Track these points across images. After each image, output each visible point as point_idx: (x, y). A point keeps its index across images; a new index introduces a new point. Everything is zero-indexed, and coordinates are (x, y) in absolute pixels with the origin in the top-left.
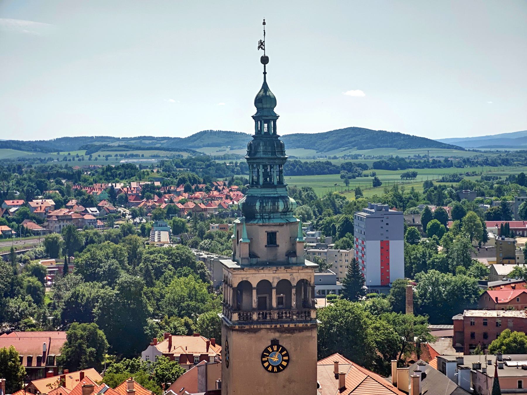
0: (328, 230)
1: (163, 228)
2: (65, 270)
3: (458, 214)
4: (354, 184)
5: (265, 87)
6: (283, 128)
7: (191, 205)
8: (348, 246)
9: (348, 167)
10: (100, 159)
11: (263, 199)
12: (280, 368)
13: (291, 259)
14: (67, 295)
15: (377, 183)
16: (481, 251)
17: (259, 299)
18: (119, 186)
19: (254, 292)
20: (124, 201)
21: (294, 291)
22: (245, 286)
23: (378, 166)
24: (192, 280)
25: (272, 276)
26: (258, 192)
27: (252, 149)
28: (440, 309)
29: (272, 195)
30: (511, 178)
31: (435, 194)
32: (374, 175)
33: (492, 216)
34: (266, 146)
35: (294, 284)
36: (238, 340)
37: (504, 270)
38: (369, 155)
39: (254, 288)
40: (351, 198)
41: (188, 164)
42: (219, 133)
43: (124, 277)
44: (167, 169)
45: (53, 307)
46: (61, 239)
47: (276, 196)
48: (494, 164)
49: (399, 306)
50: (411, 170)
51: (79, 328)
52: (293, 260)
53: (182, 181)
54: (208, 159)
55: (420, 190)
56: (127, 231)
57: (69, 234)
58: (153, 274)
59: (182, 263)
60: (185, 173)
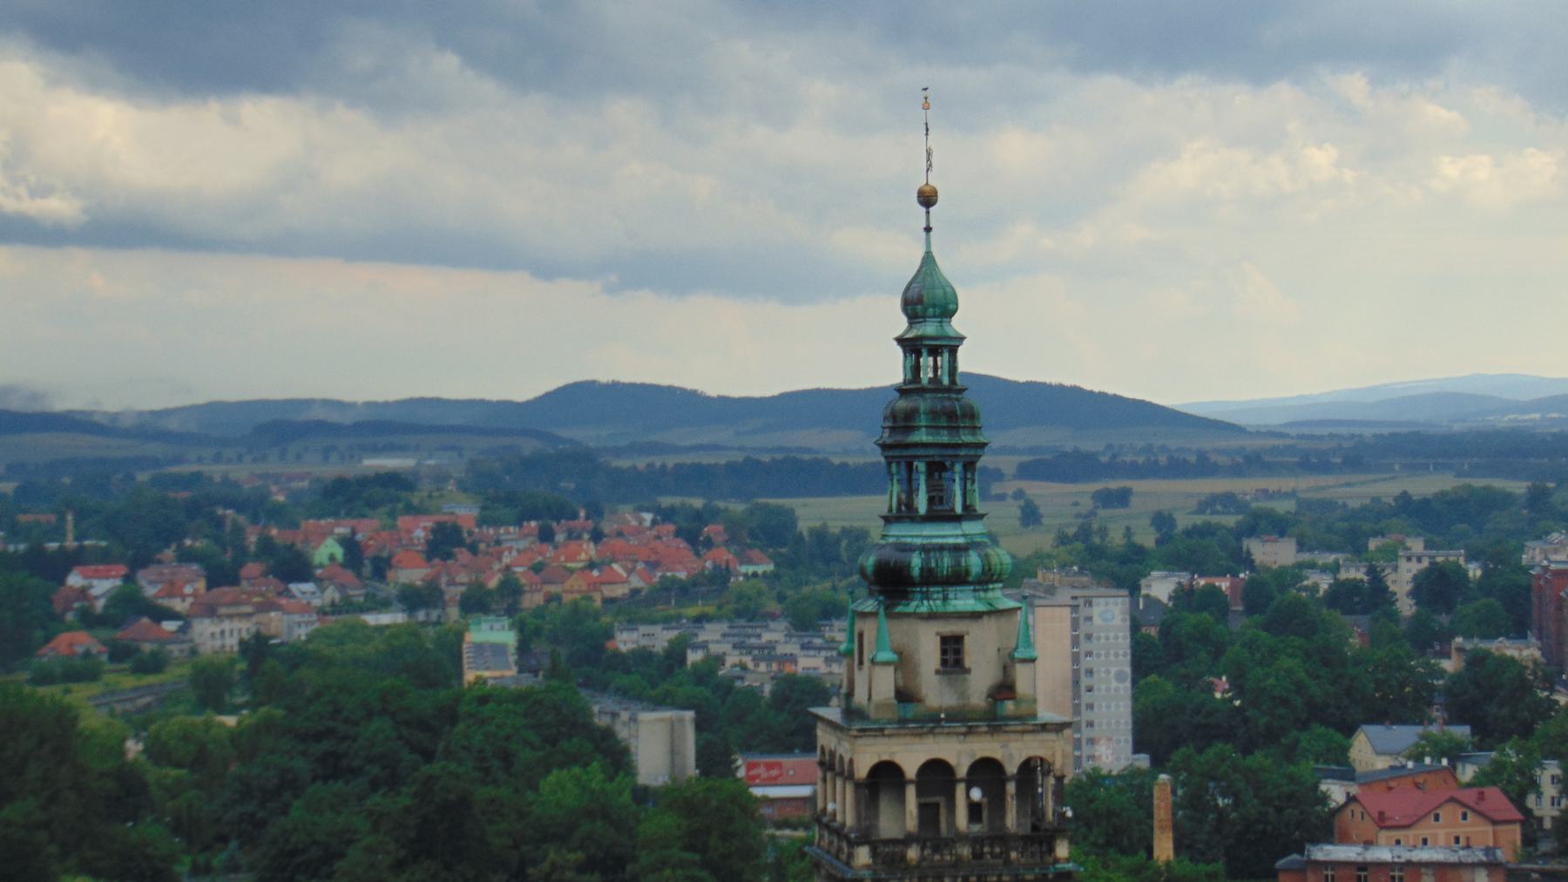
5: (928, 259)
17: (922, 807)
19: (911, 792)
21: (1011, 788)
25: (959, 753)
29: (951, 541)
32: (1019, 494)
35: (1012, 769)
39: (911, 782)
47: (961, 541)
48: (1236, 471)
50: (1114, 485)
52: (1009, 706)
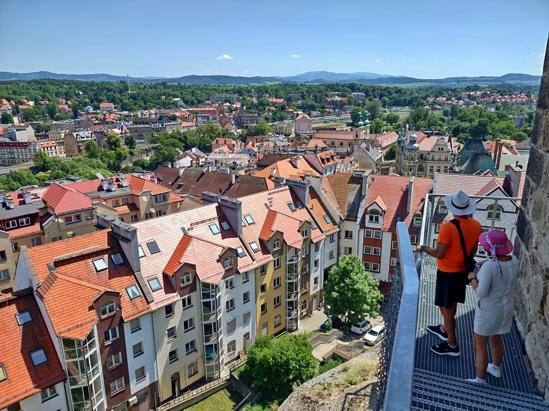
1: (492, 107)
7: (503, 100)
10: (463, 85)
18: (472, 93)
42: (516, 74)
46: (450, 110)
54: (510, 84)
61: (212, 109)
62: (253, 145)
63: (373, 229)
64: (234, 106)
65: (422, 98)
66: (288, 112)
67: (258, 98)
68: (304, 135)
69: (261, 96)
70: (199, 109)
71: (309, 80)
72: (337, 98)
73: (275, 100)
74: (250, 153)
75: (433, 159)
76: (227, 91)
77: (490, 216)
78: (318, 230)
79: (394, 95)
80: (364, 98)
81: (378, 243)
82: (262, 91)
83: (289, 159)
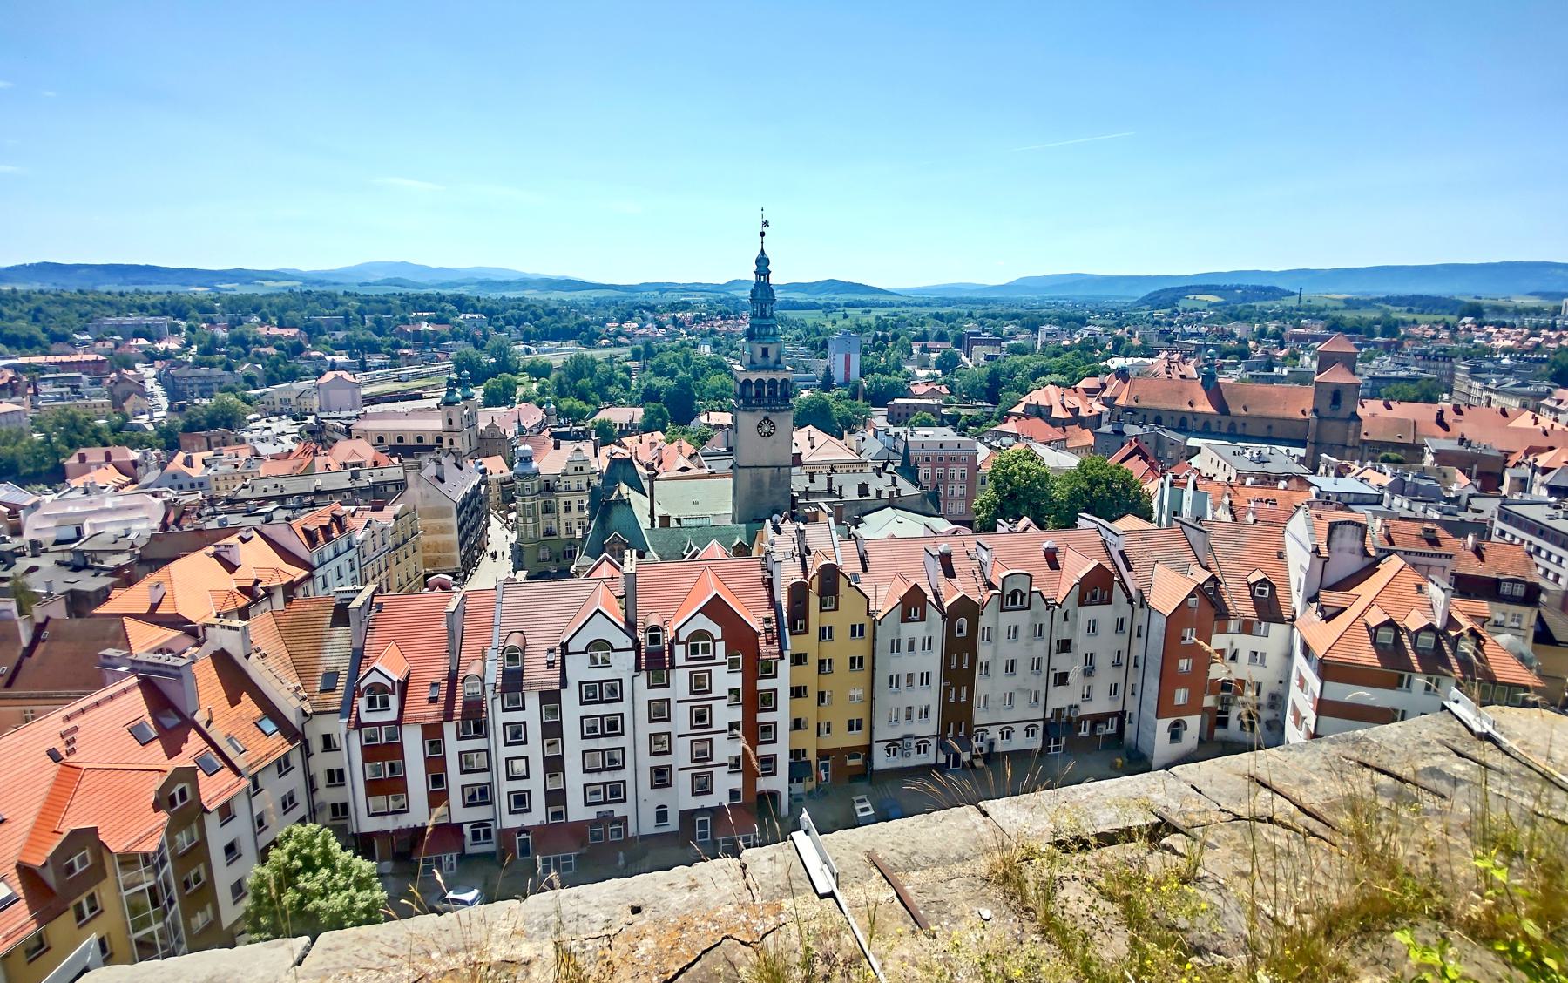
0: (813, 347)
1: (706, 343)
2: (644, 369)
3: (895, 337)
4: (831, 317)
6: (774, 279)
8: (825, 357)
9: (828, 305)
10: (668, 298)
11: (760, 326)
12: (769, 434)
13: (777, 366)
14: (644, 385)
15: (846, 316)
16: (908, 361)
20: (682, 325)
22: (747, 382)
23: (847, 305)
24: (724, 377)
25: (765, 376)
26: (756, 321)
27: (753, 293)
28: (879, 398)
30: (931, 315)
31: (882, 325)
33: (916, 340)
34: (763, 290)
36: (742, 416)
37: (922, 374)
38: (842, 298)
40: (829, 326)
41: (720, 303)
43: (681, 374)
44: (711, 305)
45: (636, 392)
49: (854, 397)
51: (652, 406)
53: (719, 313)
55: (873, 322)
56: (684, 344)
57: (647, 345)
58: (699, 373)
59: (718, 366)
60: (722, 307)
61: (91, 357)
62: (188, 463)
63: (380, 724)
64: (161, 346)
65: (597, 323)
66: (309, 358)
67: (232, 325)
68: (332, 422)
69: (240, 323)
70: (51, 359)
71: (371, 280)
72: (424, 326)
73: (275, 331)
74: (176, 483)
75: (568, 489)
76: (142, 308)
77: (594, 660)
78: (227, 771)
79: (545, 319)
80: (485, 325)
81: (394, 750)
82: (240, 309)
83: (211, 549)
